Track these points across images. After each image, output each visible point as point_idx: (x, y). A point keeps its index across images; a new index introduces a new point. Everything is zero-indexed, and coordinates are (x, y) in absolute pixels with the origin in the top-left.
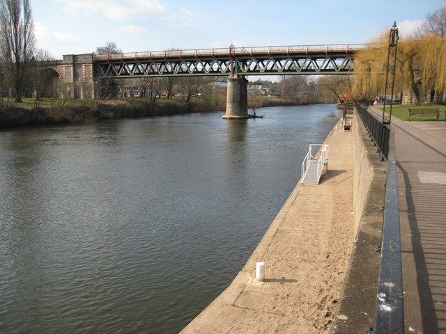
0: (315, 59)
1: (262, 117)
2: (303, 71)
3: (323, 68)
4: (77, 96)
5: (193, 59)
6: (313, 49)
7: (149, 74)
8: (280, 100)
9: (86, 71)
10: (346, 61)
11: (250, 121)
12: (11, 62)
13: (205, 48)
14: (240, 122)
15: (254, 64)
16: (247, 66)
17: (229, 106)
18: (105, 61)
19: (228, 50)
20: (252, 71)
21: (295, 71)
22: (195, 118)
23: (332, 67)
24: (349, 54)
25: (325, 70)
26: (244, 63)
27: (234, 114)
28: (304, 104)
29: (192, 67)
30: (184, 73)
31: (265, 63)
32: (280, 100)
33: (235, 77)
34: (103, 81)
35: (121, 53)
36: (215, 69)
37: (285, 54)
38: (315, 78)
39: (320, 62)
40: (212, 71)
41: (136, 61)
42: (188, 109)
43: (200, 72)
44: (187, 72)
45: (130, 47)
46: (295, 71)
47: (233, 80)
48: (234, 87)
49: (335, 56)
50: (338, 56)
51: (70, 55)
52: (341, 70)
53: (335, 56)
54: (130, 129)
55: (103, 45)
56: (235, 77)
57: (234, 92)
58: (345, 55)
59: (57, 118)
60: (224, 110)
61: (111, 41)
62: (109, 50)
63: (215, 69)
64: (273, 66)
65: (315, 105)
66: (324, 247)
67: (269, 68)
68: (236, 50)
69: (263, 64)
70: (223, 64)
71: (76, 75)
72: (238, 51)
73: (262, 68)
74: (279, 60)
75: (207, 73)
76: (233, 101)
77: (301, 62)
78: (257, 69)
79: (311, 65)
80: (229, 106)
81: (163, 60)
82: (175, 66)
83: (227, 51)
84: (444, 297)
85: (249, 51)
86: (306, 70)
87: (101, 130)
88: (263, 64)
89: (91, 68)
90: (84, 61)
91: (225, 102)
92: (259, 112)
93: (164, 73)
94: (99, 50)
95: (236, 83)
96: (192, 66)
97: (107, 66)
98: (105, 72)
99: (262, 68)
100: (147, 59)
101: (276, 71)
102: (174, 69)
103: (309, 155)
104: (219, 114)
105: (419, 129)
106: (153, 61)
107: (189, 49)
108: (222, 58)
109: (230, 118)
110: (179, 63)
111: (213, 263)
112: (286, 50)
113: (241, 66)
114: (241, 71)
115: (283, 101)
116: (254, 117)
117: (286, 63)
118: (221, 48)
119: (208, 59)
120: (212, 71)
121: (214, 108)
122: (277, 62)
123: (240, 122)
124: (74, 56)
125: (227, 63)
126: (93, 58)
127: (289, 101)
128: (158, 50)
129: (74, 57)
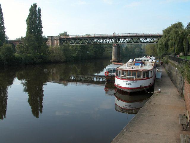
0: (146, 38)
10: (144, 39)
18: (64, 39)
20: (101, 43)
23: (146, 42)
26: (119, 39)
27: (115, 59)
30: (95, 43)
33: (116, 45)
35: (68, 35)
40: (106, 43)
46: (132, 43)
47: (115, 46)
52: (149, 43)
56: (116, 45)
61: (65, 31)
62: (65, 34)
66: (157, 103)
70: (104, 40)
72: (116, 35)
75: (98, 44)
83: (113, 35)
85: (120, 35)
89: (59, 41)
90: (56, 39)
96: (104, 41)
97: (65, 40)
101: (125, 43)
103: (39, 112)
108: (110, 38)
113: (118, 40)
117: (128, 40)
118: (110, 33)
119: (104, 38)
120: (106, 43)
124: (52, 36)
125: (106, 40)
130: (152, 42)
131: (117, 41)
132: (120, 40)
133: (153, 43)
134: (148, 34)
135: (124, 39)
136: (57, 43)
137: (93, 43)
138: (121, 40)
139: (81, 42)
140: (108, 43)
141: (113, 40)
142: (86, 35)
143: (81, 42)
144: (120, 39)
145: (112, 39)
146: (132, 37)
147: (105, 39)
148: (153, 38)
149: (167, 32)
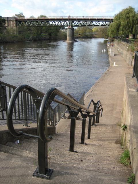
0: (99, 21)
2: (82, 25)
3: (95, 25)
5: (54, 20)
7: (27, 25)
10: (97, 22)
13: (59, 16)
19: (68, 17)
23: (98, 25)
26: (73, 22)
27: (69, 41)
30: (39, 25)
31: (61, 22)
33: (70, 27)
34: (19, 28)
35: (24, 17)
36: (56, 24)
37: (89, 19)
43: (57, 25)
45: (27, 15)
49: (86, 20)
50: (107, 21)
51: (6, 17)
52: (101, 26)
53: (86, 20)
55: (18, 13)
58: (109, 21)
60: (66, 39)
62: (20, 16)
63: (62, 24)
64: (77, 24)
67: (76, 24)
70: (54, 22)
72: (71, 18)
76: (70, 36)
77: (81, 22)
79: (98, 23)
81: (36, 20)
83: (67, 18)
85: (75, 18)
87: (68, 48)
89: (15, 22)
95: (71, 29)
97: (21, 22)
98: (20, 24)
99: (66, 24)
105: (33, 48)
106: (34, 21)
108: (65, 20)
111: (104, 148)
114: (72, 25)
120: (55, 25)
121: (64, 38)
124: (8, 17)
125: (55, 22)
126: (15, 18)
130: (104, 26)
134: (87, 18)
135: (79, 21)
136: (13, 23)
137: (38, 25)
138: (62, 22)
139: (32, 23)
141: (68, 22)
142: (42, 16)
143: (32, 23)
145: (67, 22)
146: (86, 20)
147: (54, 21)
148: (105, 22)
149: (119, 16)
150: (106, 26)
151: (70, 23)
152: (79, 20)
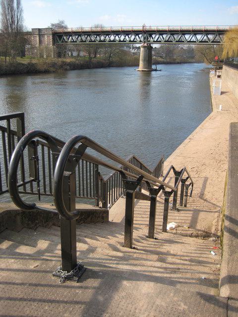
0: (195, 34)
1: (160, 70)
2: (177, 42)
4: (42, 56)
6: (160, 28)
8: (163, 60)
9: (48, 40)
10: (191, 36)
11: (153, 73)
12: (9, 32)
13: (117, 27)
14: (147, 73)
15: (133, 37)
16: (153, 38)
17: (141, 63)
20: (132, 41)
21: (172, 42)
22: (113, 71)
23: (195, 40)
24: (220, 32)
25: (190, 41)
26: (151, 36)
27: (144, 68)
28: (178, 63)
29: (89, 38)
31: (130, 36)
32: (163, 60)
33: (146, 45)
36: (122, 40)
37: (119, 31)
38: (185, 46)
39: (187, 37)
40: (120, 41)
41: (79, 34)
42: (108, 64)
44: (95, 41)
45: (72, 25)
46: (172, 42)
48: (145, 51)
50: (211, 33)
52: (200, 42)
54: (72, 76)
55: (56, 22)
57: (145, 55)
59: (43, 68)
60: (138, 65)
61: (61, 20)
62: (60, 26)
65: (186, 64)
67: (132, 40)
68: (147, 28)
69: (163, 37)
71: (40, 42)
72: (148, 28)
73: (138, 39)
74: (162, 35)
76: (144, 60)
77: (176, 36)
78: (135, 40)
80: (141, 63)
81: (88, 33)
82: (78, 37)
83: (141, 28)
84: (3, 266)
85: (154, 28)
86: (179, 41)
88: (163, 37)
89: (51, 37)
90: (46, 33)
91: (139, 60)
92: (159, 67)
93: (71, 42)
94: (53, 25)
99: (138, 39)
100: (79, 32)
101: (160, 41)
102: (77, 39)
104: (135, 68)
107: (107, 27)
108: (137, 33)
109: (142, 71)
110: (80, 35)
112: (166, 28)
114: (149, 41)
115: (165, 60)
116: (156, 70)
117: (166, 37)
118: (138, 27)
120: (120, 41)
122: (137, 37)
123: (147, 73)
124: (39, 29)
125: (119, 36)
127: (168, 60)
128: (87, 26)
129: (39, 30)
131: (148, 38)
132: (153, 36)
133: (207, 42)
135: (160, 34)
140: (123, 41)
141: (142, 37)
144: (152, 34)
145: (140, 36)
150: (207, 42)
151: (145, 38)
152: (161, 32)
